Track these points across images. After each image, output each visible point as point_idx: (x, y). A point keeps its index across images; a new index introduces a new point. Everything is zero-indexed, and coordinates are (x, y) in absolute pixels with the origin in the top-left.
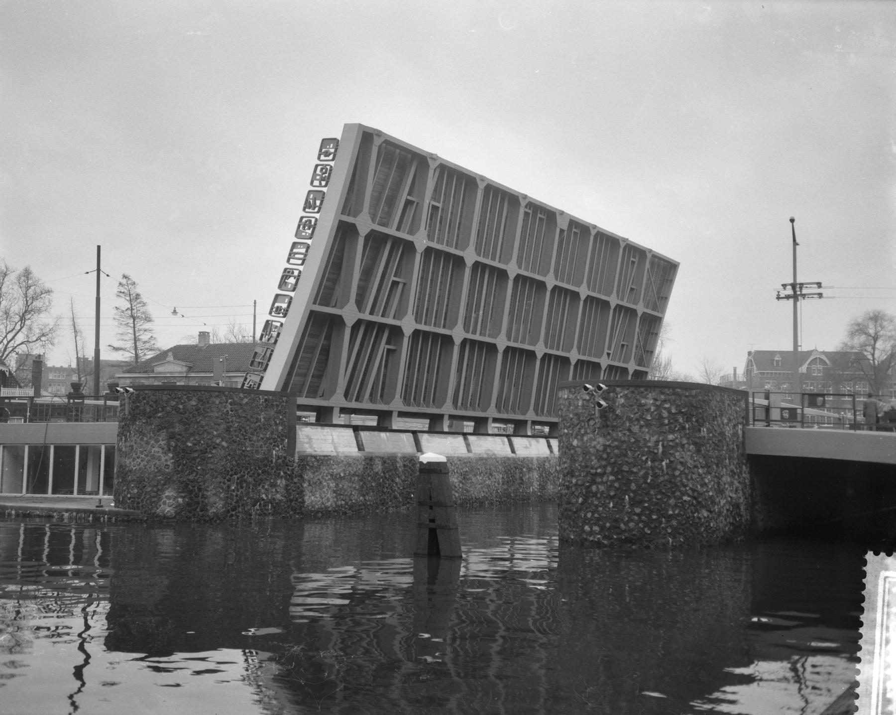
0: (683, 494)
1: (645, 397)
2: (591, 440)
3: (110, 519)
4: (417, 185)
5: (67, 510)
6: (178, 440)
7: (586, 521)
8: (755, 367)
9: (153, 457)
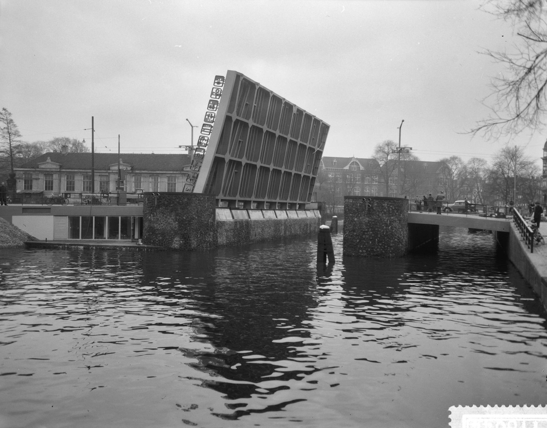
0: (395, 238)
1: (384, 203)
2: (363, 219)
3: (147, 250)
4: (251, 97)
5: (124, 247)
6: (180, 216)
7: (360, 248)
8: (323, 165)
9: (169, 223)
